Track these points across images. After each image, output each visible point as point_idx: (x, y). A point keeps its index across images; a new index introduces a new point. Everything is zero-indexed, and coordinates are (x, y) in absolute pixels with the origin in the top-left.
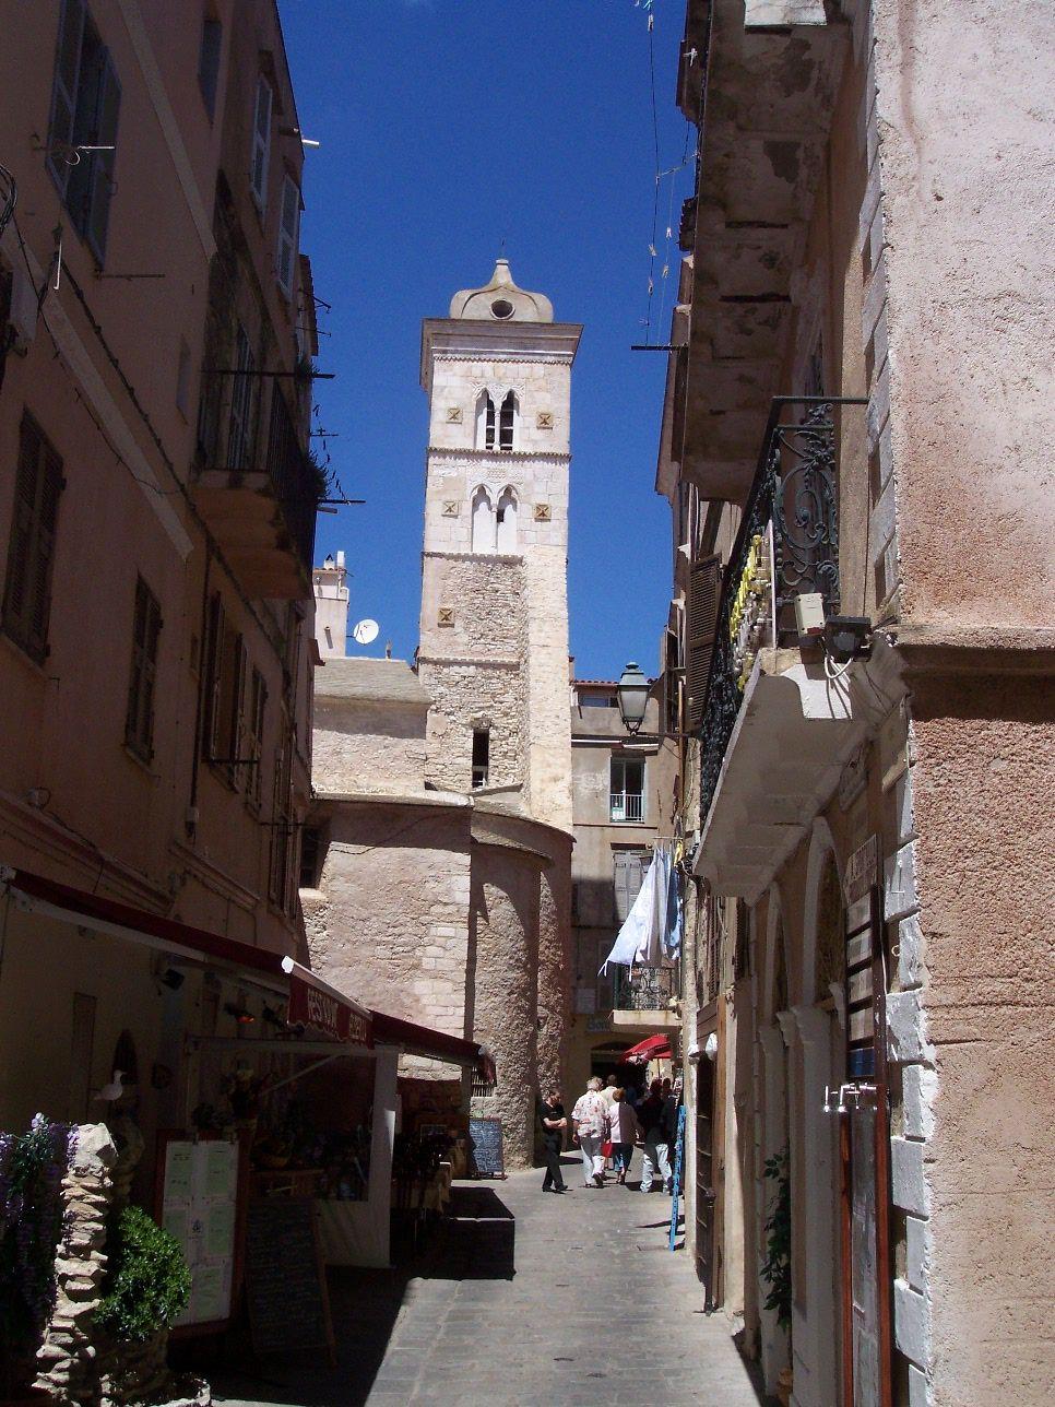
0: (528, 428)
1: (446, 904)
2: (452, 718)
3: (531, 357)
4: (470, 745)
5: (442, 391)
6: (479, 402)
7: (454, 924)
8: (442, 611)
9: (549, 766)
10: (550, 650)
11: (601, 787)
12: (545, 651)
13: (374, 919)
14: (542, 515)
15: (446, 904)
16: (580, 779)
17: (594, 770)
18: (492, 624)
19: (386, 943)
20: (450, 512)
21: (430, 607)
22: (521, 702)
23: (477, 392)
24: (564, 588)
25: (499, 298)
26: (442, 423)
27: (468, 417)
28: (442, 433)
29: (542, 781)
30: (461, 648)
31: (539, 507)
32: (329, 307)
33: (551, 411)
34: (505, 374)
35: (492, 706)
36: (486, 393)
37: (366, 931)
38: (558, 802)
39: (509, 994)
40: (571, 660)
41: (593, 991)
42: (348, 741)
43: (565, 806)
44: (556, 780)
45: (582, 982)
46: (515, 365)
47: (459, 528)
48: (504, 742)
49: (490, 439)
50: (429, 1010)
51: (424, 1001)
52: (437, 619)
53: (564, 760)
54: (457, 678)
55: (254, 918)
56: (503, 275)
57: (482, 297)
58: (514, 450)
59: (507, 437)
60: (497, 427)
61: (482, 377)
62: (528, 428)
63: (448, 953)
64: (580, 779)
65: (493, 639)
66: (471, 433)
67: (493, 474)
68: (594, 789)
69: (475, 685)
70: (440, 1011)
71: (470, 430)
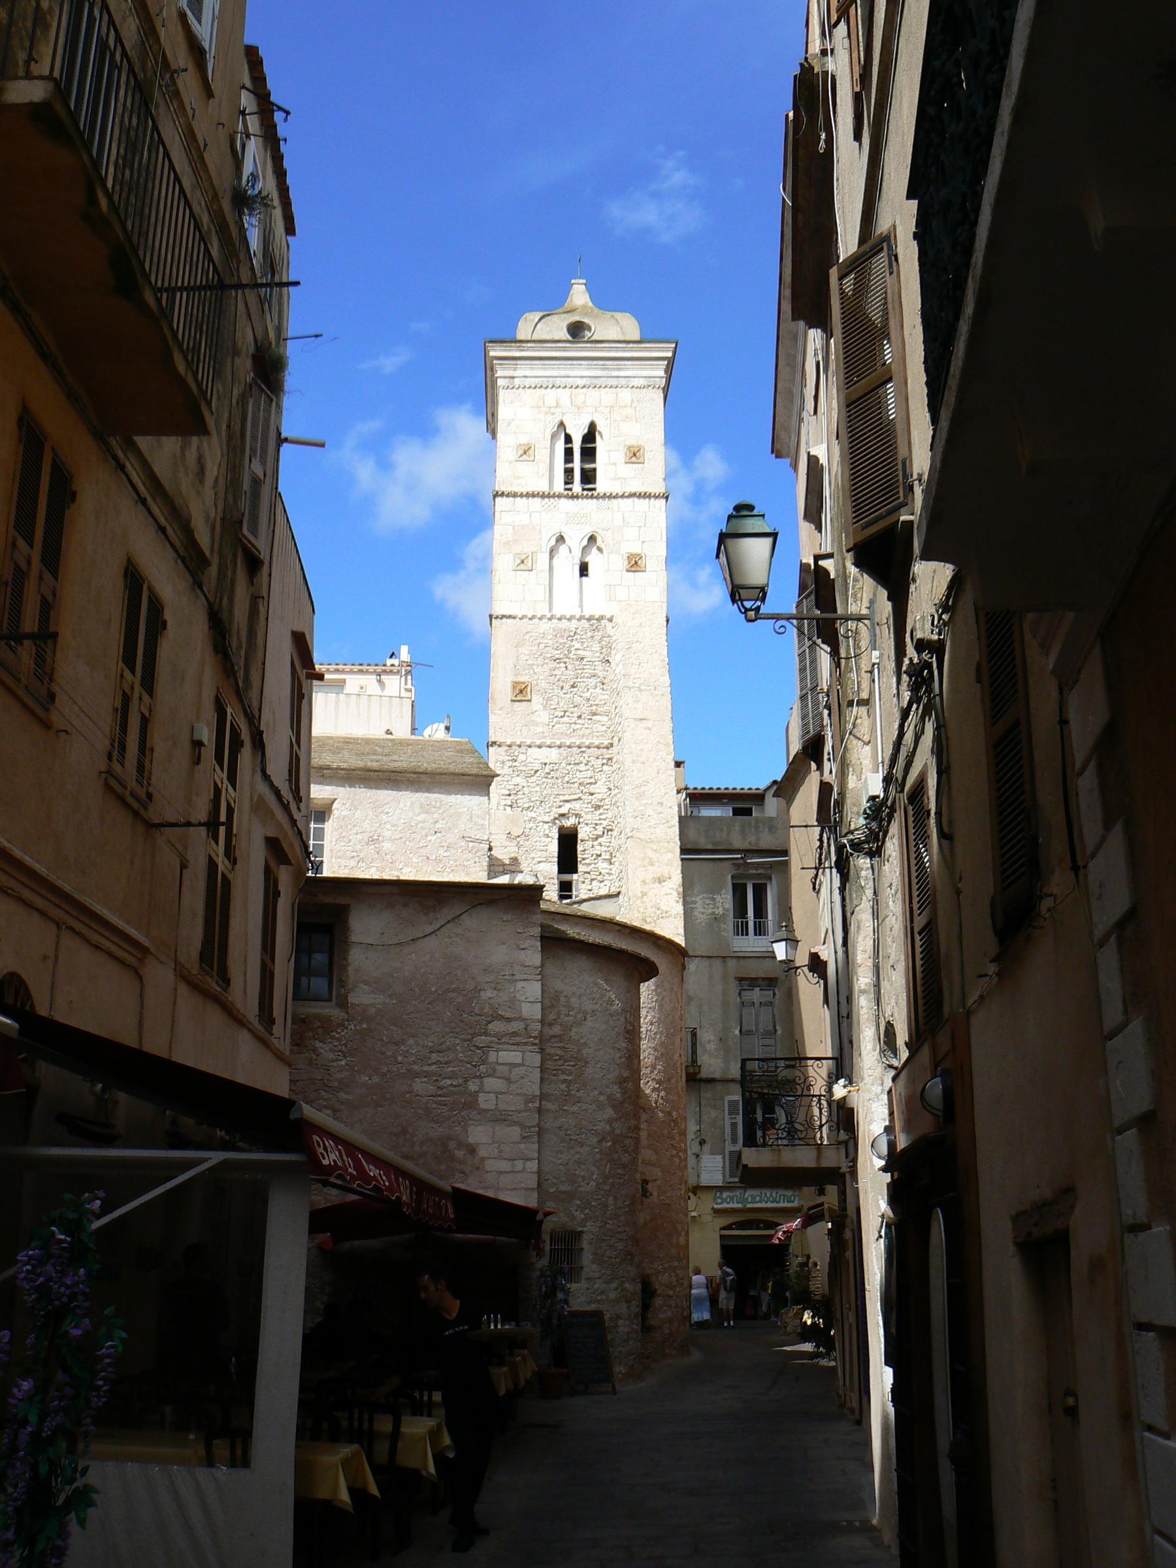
0: (615, 464)
1: (509, 1020)
2: (532, 814)
3: (614, 382)
4: (554, 847)
5: (509, 424)
6: (554, 436)
7: (521, 1048)
8: (515, 684)
9: (652, 864)
10: (650, 724)
11: (720, 911)
12: (644, 724)
13: (411, 1041)
14: (635, 564)
15: (509, 1020)
16: (695, 902)
17: (712, 892)
18: (577, 699)
19: (427, 1075)
20: (524, 563)
21: (501, 683)
22: (617, 791)
23: (552, 426)
24: (664, 651)
25: (577, 318)
26: (510, 462)
27: (542, 453)
28: (509, 471)
29: (644, 882)
30: (540, 729)
31: (630, 557)
32: (288, 113)
33: (641, 443)
34: (584, 402)
35: (580, 799)
36: (562, 425)
37: (400, 1058)
38: (664, 908)
39: (600, 1142)
40: (678, 764)
41: (719, 1158)
42: (388, 826)
43: (673, 912)
44: (660, 880)
45: (707, 1147)
46: (596, 392)
47: (535, 583)
48: (595, 843)
49: (569, 480)
50: (490, 1165)
51: (482, 1152)
52: (509, 694)
53: (670, 855)
54: (537, 766)
55: (140, 978)
56: (579, 295)
57: (555, 318)
58: (598, 490)
59: (589, 477)
60: (577, 465)
61: (557, 406)
62: (615, 464)
63: (513, 1087)
64: (695, 902)
65: (579, 717)
66: (545, 469)
67: (576, 517)
68: (713, 913)
69: (558, 774)
70: (504, 1165)
71: (544, 467)
